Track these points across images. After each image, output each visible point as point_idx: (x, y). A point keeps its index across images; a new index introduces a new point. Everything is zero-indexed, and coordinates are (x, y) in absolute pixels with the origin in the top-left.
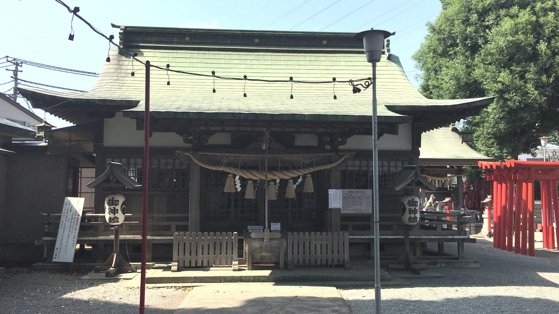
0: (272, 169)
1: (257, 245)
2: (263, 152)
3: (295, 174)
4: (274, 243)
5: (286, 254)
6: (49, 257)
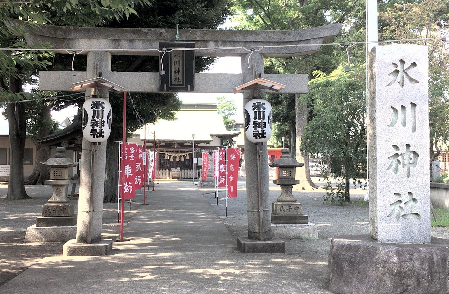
0: (178, 152)
1: (173, 173)
2: (175, 148)
3: (184, 154)
4: (178, 172)
5: (181, 176)
6: (81, 264)
